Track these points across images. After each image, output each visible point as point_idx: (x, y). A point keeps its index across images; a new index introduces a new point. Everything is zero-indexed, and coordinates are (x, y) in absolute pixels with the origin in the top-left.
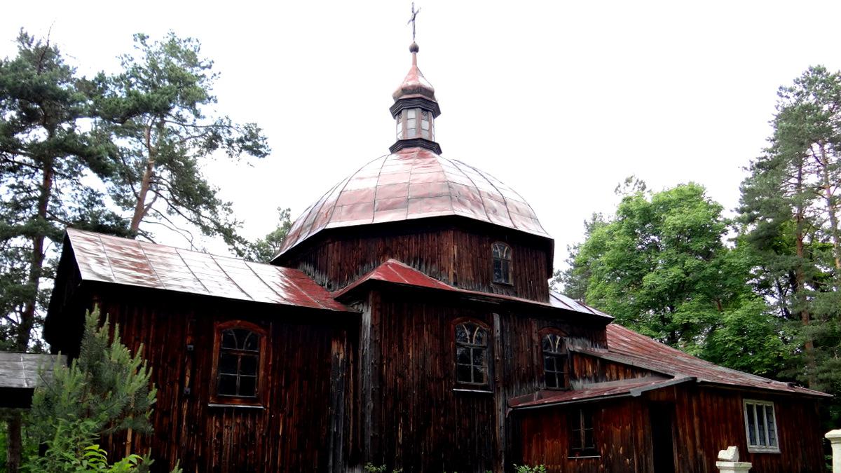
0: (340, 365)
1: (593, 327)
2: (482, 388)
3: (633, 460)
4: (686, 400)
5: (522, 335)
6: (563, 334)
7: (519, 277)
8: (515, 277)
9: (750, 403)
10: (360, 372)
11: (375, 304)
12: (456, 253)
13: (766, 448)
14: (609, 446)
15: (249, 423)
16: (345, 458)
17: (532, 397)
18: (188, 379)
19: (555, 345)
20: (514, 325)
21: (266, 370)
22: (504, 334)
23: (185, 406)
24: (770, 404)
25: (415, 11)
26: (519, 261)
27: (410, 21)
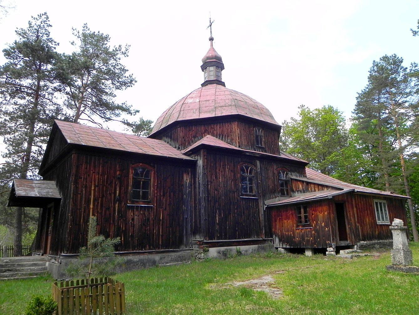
0: (188, 186)
1: (300, 167)
2: (253, 196)
3: (329, 228)
4: (349, 199)
5: (269, 171)
7: (267, 144)
8: (265, 143)
10: (197, 188)
13: (384, 222)
14: (317, 222)
15: (146, 213)
16: (191, 231)
18: (118, 192)
19: (284, 177)
20: (266, 166)
21: (154, 188)
22: (262, 171)
23: (117, 205)
24: (385, 201)
25: (211, 22)
26: (266, 136)
27: (209, 27)
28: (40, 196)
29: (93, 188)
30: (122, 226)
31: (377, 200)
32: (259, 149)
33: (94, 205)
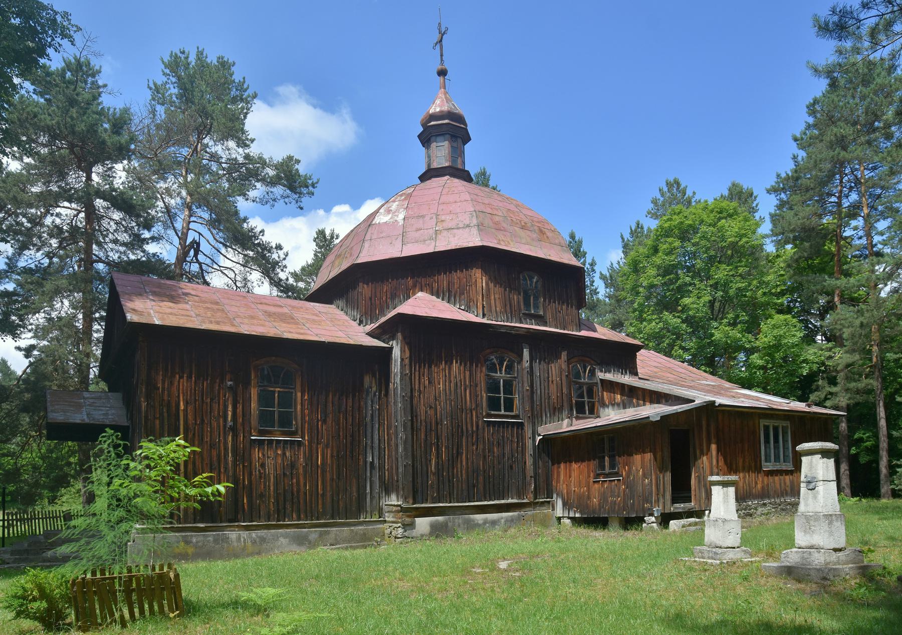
3: (651, 480)
6: (592, 362)
9: (766, 424)
11: (404, 338)
12: (484, 285)
14: (630, 469)
17: (562, 425)
18: (230, 413)
23: (230, 438)
24: (787, 424)
28: (91, 422)
29: (182, 407)
31: (768, 421)
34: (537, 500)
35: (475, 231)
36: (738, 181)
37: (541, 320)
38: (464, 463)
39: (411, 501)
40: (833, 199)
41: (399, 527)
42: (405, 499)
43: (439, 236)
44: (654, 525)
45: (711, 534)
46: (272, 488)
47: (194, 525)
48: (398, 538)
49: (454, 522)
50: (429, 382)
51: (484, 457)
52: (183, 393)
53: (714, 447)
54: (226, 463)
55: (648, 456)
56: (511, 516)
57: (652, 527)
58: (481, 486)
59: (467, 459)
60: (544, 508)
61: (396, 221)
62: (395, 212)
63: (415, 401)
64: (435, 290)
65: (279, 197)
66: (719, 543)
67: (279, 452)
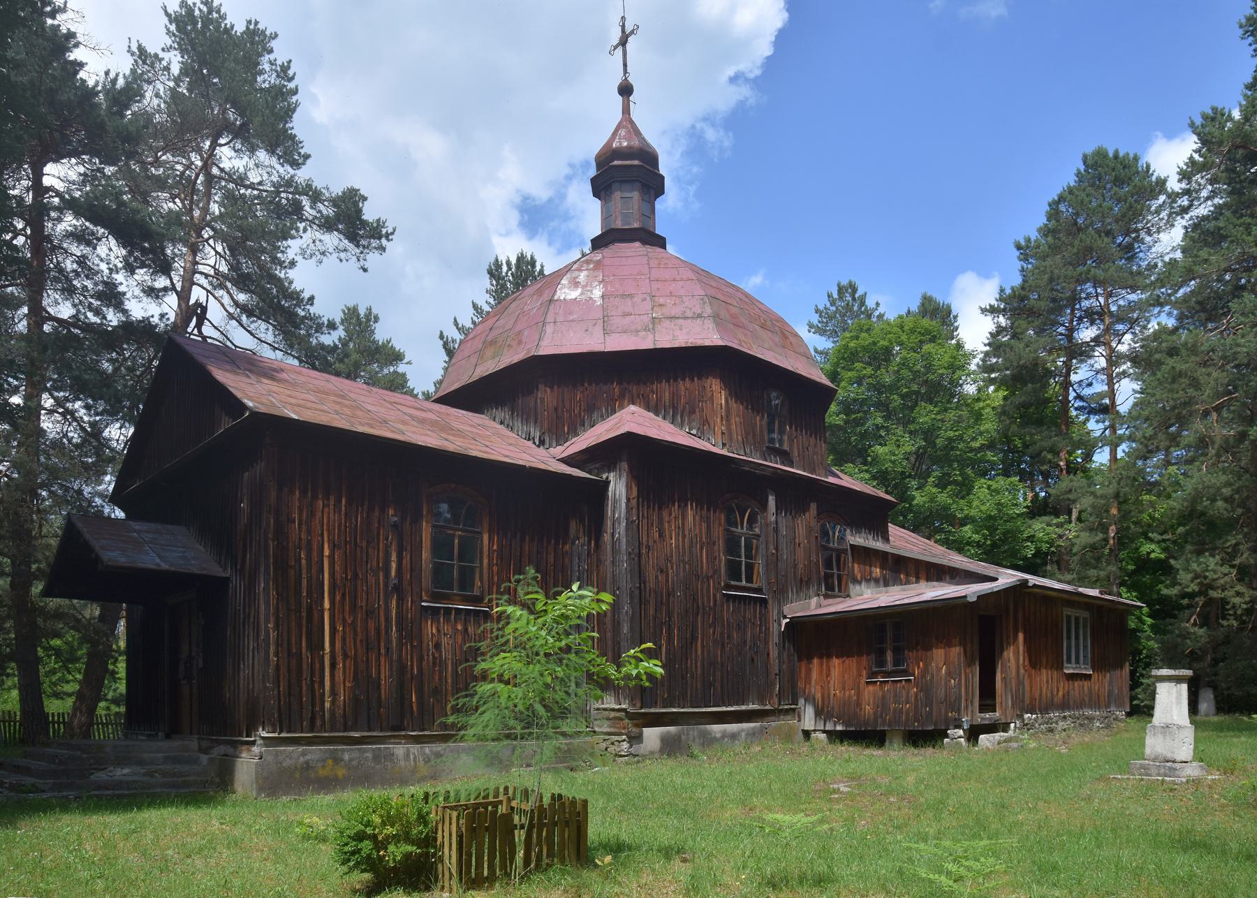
3: (960, 680)
11: (631, 470)
17: (809, 604)
18: (394, 565)
23: (394, 603)
24: (1086, 614)
29: (327, 552)
30: (412, 661)
32: (775, 457)
33: (332, 602)
34: (781, 707)
35: (710, 324)
36: (931, 293)
37: (786, 457)
38: (699, 653)
39: (639, 705)
40: (1061, 330)
41: (624, 740)
42: (632, 703)
43: (658, 327)
44: (962, 740)
45: (1155, 744)
46: (449, 681)
47: (345, 734)
48: (621, 756)
49: (688, 734)
50: (660, 536)
51: (723, 644)
52: (328, 530)
53: (1021, 636)
54: (389, 641)
55: (956, 651)
56: (753, 728)
57: (960, 744)
58: (718, 684)
59: (703, 647)
60: (789, 717)
61: (590, 298)
62: (586, 286)
63: (643, 562)
64: (653, 403)
65: (331, 250)
66: (1169, 756)
67: (459, 627)
